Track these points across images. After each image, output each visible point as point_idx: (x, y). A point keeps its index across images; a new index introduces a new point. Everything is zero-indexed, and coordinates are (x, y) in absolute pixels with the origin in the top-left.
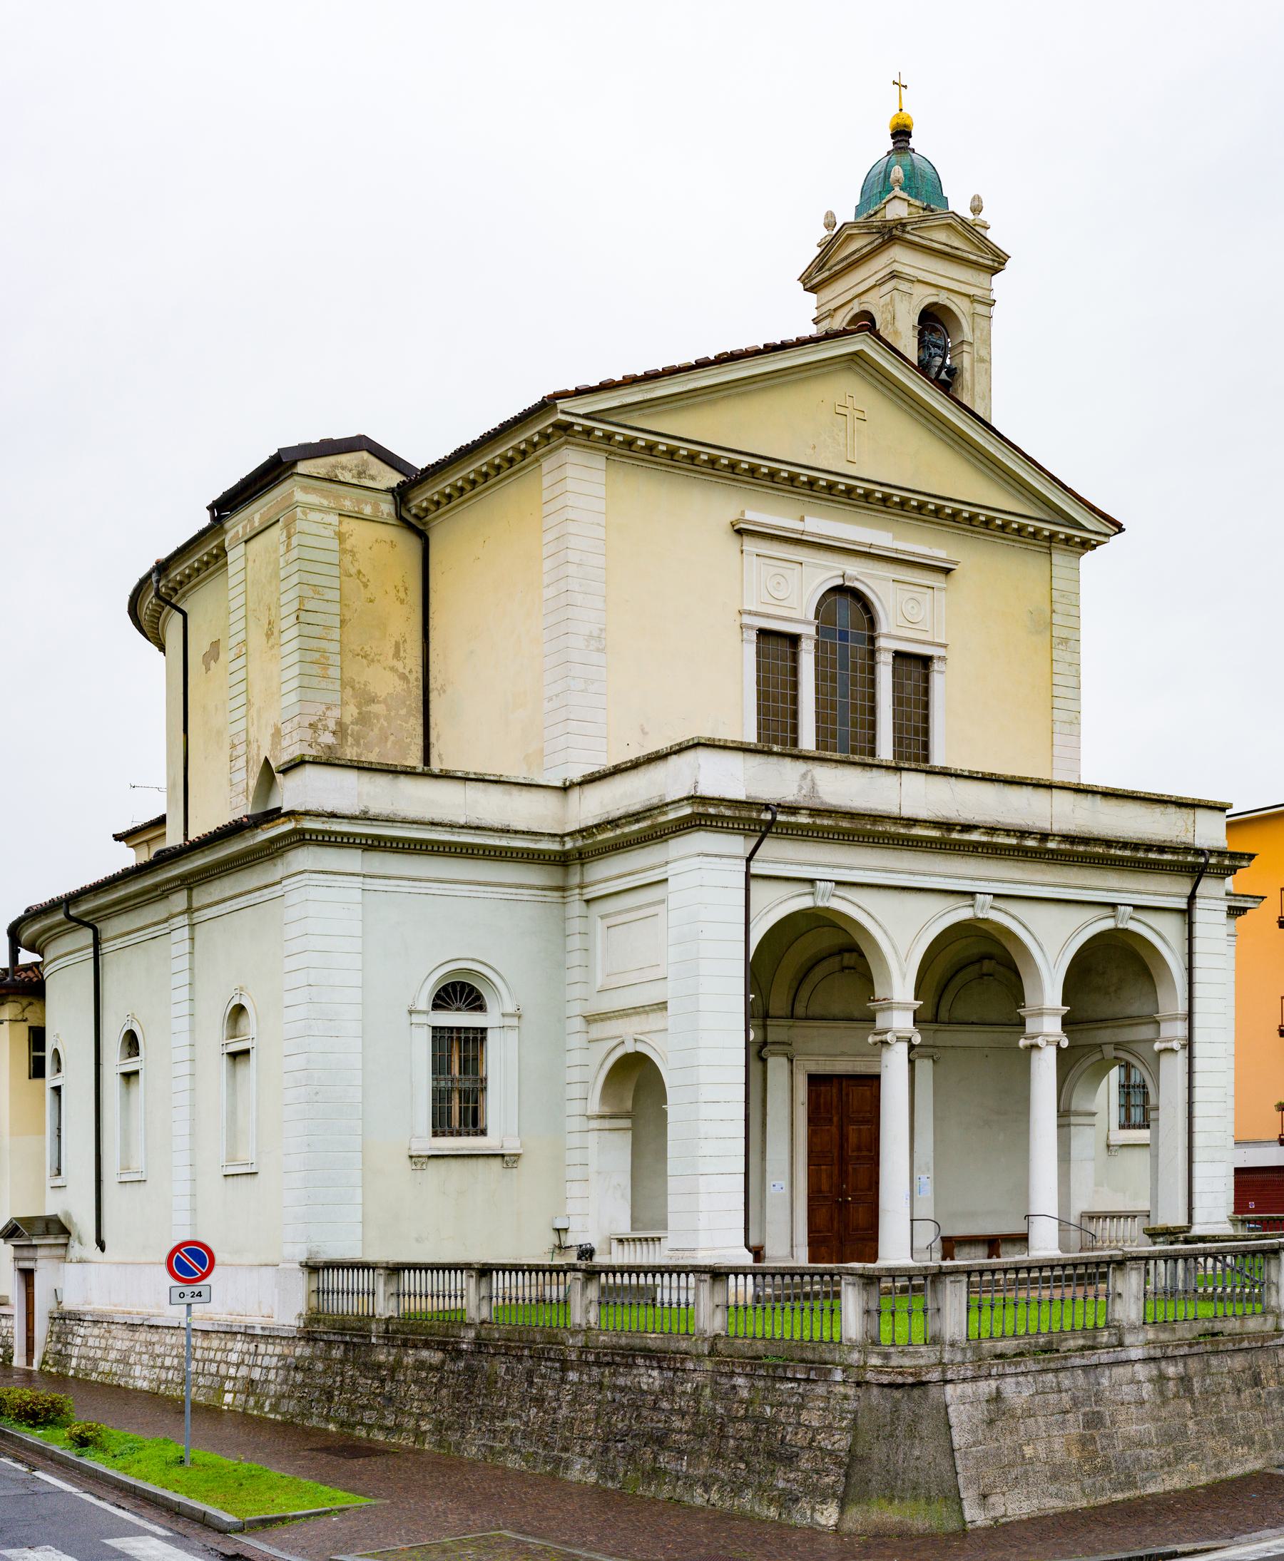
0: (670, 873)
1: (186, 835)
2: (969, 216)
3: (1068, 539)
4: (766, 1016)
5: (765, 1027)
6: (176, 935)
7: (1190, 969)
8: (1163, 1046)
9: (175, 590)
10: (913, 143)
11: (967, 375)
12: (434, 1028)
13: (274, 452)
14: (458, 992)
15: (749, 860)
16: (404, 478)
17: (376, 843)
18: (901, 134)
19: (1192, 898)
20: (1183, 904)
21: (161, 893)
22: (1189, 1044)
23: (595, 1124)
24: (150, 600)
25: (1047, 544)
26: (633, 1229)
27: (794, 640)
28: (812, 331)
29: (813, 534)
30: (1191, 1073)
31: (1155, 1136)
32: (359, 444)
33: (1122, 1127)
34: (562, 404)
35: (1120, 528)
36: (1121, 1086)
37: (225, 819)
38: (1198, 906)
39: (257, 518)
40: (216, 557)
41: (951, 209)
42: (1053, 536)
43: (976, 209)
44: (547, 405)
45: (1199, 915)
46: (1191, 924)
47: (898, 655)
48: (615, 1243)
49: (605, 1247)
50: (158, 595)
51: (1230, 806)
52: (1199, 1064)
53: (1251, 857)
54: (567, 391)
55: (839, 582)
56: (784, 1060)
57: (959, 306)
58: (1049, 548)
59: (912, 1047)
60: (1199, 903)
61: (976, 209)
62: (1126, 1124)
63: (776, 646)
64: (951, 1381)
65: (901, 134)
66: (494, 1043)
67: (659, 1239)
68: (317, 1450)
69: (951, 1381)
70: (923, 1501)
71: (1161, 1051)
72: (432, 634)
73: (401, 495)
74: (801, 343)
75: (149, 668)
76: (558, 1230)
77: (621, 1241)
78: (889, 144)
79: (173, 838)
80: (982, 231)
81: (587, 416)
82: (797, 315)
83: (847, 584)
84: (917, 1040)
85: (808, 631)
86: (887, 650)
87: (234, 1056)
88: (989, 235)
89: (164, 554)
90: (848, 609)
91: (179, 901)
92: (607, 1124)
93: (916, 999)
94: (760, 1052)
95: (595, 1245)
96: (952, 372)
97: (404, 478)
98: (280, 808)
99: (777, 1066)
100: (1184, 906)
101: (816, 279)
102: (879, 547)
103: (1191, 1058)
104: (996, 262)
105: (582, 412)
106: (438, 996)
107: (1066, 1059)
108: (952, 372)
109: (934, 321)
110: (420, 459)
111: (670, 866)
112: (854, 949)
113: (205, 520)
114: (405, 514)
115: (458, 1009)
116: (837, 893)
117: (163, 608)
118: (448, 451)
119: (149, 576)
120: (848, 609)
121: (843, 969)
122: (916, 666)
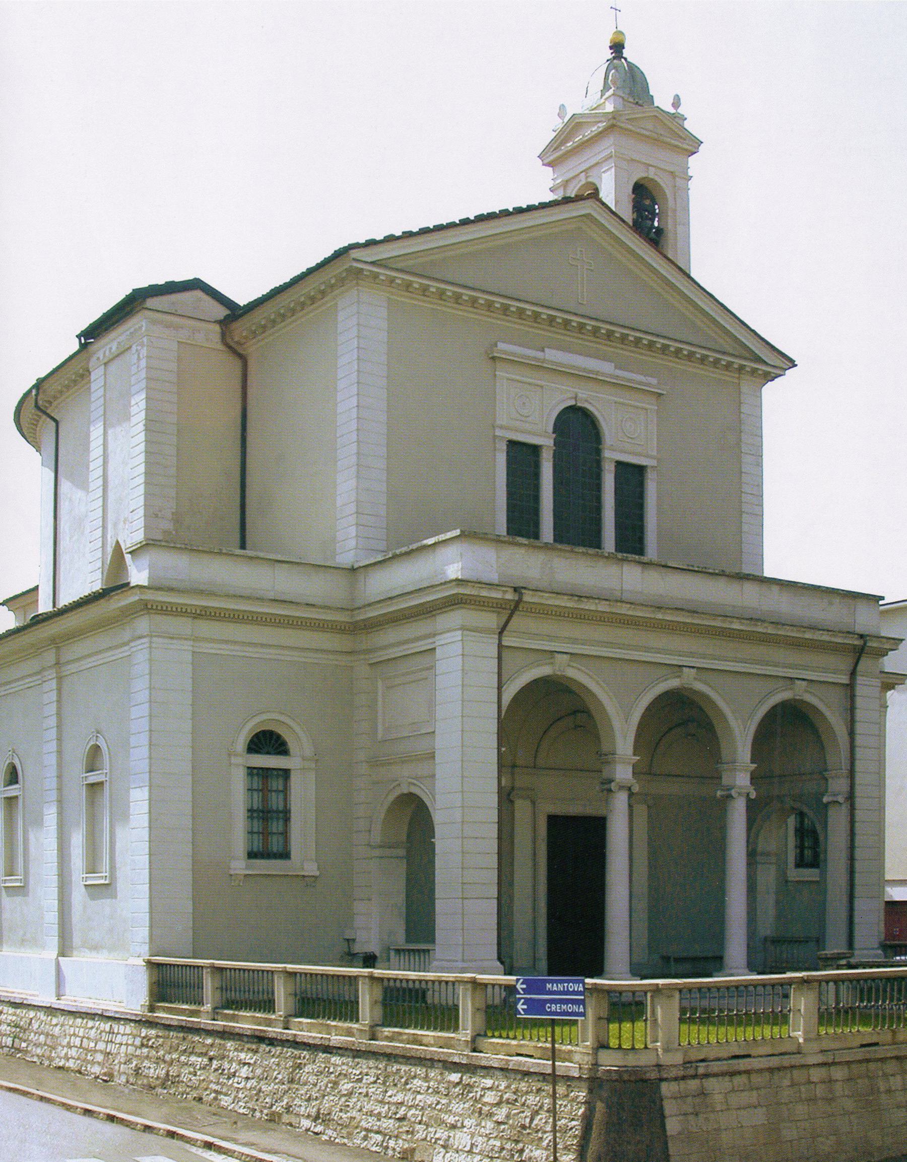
0: (437, 644)
1: (54, 606)
2: (672, 111)
3: (754, 371)
4: (514, 766)
5: (513, 774)
6: (47, 686)
7: (852, 733)
8: (830, 799)
9: (50, 403)
10: (626, 53)
11: (670, 235)
12: (248, 768)
13: (129, 291)
14: (267, 741)
15: (501, 633)
16: (228, 312)
17: (203, 613)
18: (617, 47)
19: (853, 674)
20: (845, 679)
21: (37, 650)
22: (851, 797)
23: (377, 852)
24: (29, 409)
25: (737, 375)
26: (408, 941)
27: (535, 450)
28: (549, 197)
29: (553, 363)
30: (852, 822)
31: (823, 874)
32: (196, 285)
33: (798, 866)
34: (354, 254)
35: (793, 364)
36: (796, 830)
37: (85, 590)
38: (858, 682)
39: (114, 346)
40: (82, 376)
41: (656, 105)
42: (741, 368)
43: (677, 103)
44: (339, 254)
45: (860, 691)
46: (853, 697)
47: (619, 464)
48: (392, 953)
49: (384, 955)
50: (37, 407)
51: (882, 598)
52: (859, 815)
53: (902, 640)
54: (358, 243)
55: (572, 403)
56: (527, 803)
57: (664, 181)
58: (739, 378)
59: (631, 795)
60: (860, 680)
61: (677, 103)
62: (801, 863)
63: (523, 457)
64: (666, 1080)
65: (617, 47)
66: (295, 779)
67: (429, 951)
68: (576, 694)
69: (666, 1080)
70: (477, 1115)
71: (829, 803)
72: (249, 439)
73: (225, 323)
74: (543, 206)
75: (28, 465)
76: (348, 940)
77: (398, 951)
78: (608, 54)
79: (44, 606)
80: (680, 122)
81: (373, 263)
82: (536, 186)
83: (579, 404)
84: (636, 789)
85: (546, 441)
86: (611, 460)
87: (92, 785)
88: (687, 125)
89: (43, 375)
90: (578, 429)
91: (50, 657)
92: (388, 852)
93: (634, 755)
94: (509, 795)
95: (378, 955)
96: (660, 231)
97: (228, 312)
98: (129, 583)
99: (522, 807)
100: (847, 681)
101: (556, 154)
102: (603, 374)
103: (852, 808)
104: (692, 145)
105: (370, 260)
106: (252, 741)
107: (753, 807)
108: (660, 231)
109: (644, 195)
110: (242, 300)
111: (438, 638)
112: (586, 711)
113: (76, 347)
114: (229, 340)
115: (268, 753)
116: (572, 664)
117: (40, 417)
118: (265, 290)
119: (30, 391)
120: (578, 429)
121: (576, 727)
122: (632, 477)
